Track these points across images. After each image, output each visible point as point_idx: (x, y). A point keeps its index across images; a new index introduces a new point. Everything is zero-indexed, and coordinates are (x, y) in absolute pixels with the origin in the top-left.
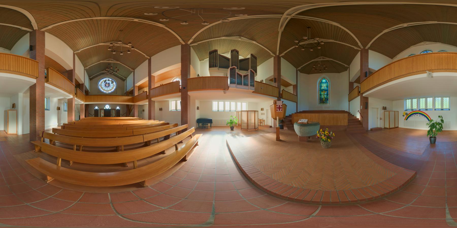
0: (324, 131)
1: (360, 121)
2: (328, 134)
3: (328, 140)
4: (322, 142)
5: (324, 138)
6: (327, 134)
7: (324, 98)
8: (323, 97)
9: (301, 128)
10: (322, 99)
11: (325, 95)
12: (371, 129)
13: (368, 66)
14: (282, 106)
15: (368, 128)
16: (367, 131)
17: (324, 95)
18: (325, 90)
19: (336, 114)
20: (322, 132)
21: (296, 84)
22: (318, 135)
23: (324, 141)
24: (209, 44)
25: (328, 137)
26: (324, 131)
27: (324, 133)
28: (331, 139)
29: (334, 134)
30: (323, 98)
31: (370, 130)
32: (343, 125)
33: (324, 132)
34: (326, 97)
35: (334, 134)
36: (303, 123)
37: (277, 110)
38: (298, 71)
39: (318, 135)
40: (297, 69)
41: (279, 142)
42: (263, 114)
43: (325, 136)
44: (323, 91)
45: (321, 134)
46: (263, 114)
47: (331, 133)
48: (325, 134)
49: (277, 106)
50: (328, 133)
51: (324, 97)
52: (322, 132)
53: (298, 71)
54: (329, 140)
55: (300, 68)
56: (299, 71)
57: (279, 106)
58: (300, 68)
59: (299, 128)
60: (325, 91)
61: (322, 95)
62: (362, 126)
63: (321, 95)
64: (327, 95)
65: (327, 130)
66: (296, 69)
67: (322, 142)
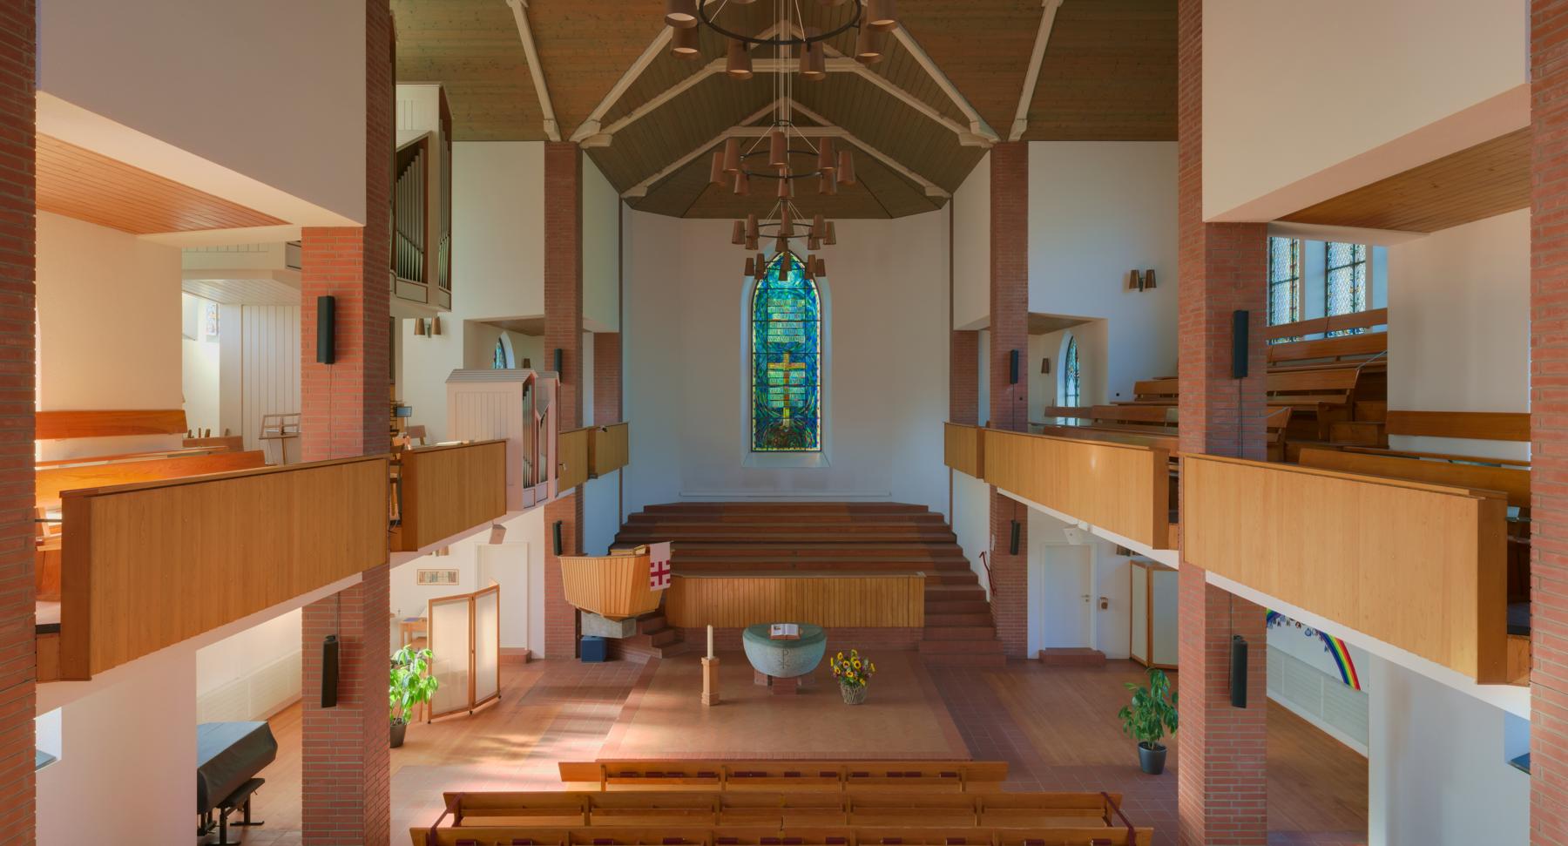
0: (847, 658)
1: (988, 603)
2: (860, 666)
3: (861, 680)
4: (844, 689)
5: (851, 676)
6: (857, 665)
7: (787, 413)
8: (781, 404)
9: (785, 652)
10: (775, 415)
11: (795, 390)
12: (1041, 652)
13: (1026, 302)
14: (668, 562)
15: (1023, 646)
16: (1018, 660)
17: (787, 385)
18: (796, 353)
19: (874, 580)
20: (842, 661)
21: (618, 331)
22: (836, 668)
23: (850, 684)
24: (437, 311)
25: (862, 674)
26: (847, 658)
27: (847, 662)
28: (866, 678)
29: (872, 665)
30: (780, 411)
31: (1037, 656)
32: (906, 625)
33: (849, 661)
34: (800, 404)
35: (872, 665)
36: (787, 636)
37: (653, 584)
38: (624, 203)
39: (836, 668)
40: (622, 196)
41: (722, 708)
42: (427, 579)
43: (852, 671)
44: (779, 360)
45: (842, 665)
46: (427, 579)
47: (866, 662)
48: (851, 666)
49: (653, 565)
50: (858, 662)
51: (786, 398)
52: (842, 661)
53: (624, 203)
54: (863, 682)
55: (640, 191)
56: (589, 156)
57: (660, 564)
58: (640, 191)
59: (781, 655)
60: (794, 358)
61: (771, 390)
62: (995, 633)
63: (763, 385)
64: (809, 384)
65: (854, 655)
66: (617, 194)
67: (844, 689)
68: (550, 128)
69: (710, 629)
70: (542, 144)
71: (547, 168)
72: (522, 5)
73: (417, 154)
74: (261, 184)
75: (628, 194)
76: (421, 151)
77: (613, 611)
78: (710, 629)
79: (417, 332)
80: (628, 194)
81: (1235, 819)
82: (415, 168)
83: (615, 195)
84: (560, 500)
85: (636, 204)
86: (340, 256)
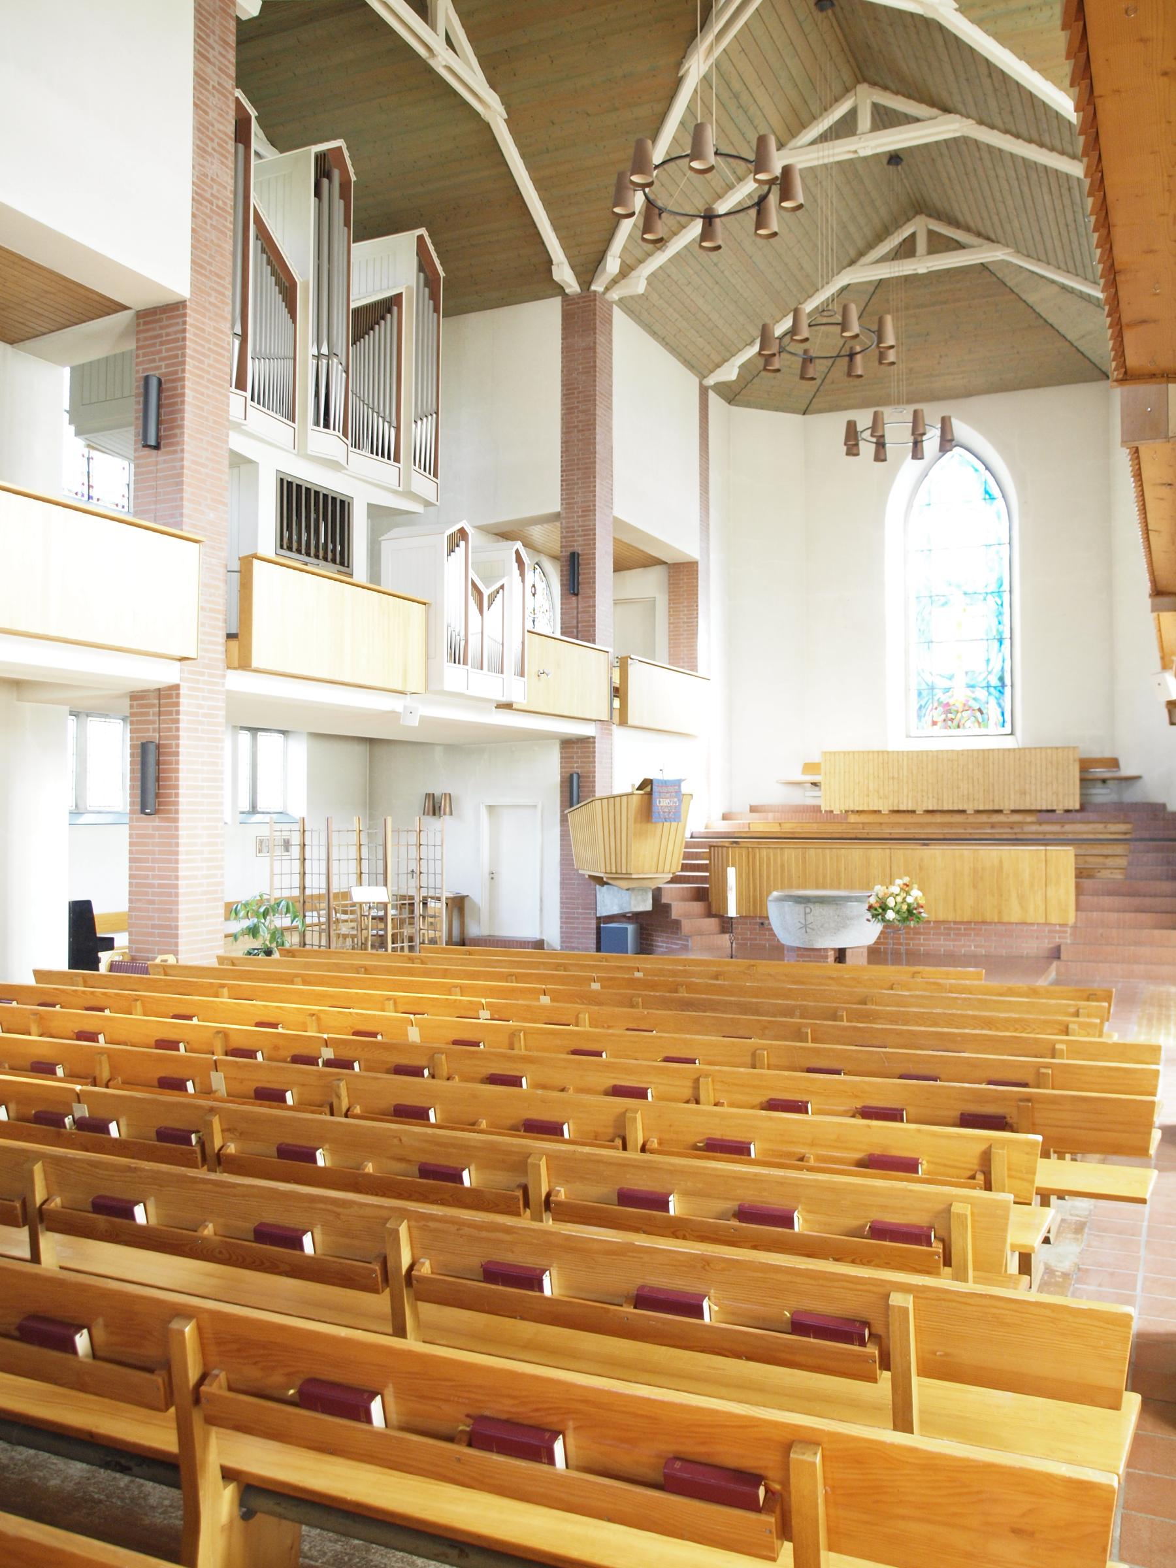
9: (808, 910)
38: (712, 396)
53: (712, 396)
68: (564, 273)
69: (707, 874)
70: (558, 300)
71: (564, 329)
72: (701, 42)
73: (389, 311)
74: (77, 240)
75: (711, 381)
76: (395, 309)
77: (633, 898)
78: (707, 874)
79: (1128, 1388)
80: (711, 381)
81: (209, 295)
82: (384, 329)
83: (690, 384)
84: (1002, 1251)
85: (733, 394)
86: (168, 335)
